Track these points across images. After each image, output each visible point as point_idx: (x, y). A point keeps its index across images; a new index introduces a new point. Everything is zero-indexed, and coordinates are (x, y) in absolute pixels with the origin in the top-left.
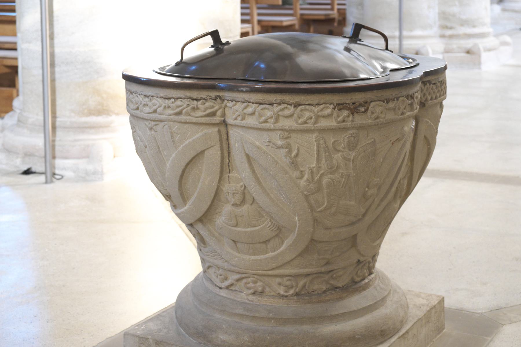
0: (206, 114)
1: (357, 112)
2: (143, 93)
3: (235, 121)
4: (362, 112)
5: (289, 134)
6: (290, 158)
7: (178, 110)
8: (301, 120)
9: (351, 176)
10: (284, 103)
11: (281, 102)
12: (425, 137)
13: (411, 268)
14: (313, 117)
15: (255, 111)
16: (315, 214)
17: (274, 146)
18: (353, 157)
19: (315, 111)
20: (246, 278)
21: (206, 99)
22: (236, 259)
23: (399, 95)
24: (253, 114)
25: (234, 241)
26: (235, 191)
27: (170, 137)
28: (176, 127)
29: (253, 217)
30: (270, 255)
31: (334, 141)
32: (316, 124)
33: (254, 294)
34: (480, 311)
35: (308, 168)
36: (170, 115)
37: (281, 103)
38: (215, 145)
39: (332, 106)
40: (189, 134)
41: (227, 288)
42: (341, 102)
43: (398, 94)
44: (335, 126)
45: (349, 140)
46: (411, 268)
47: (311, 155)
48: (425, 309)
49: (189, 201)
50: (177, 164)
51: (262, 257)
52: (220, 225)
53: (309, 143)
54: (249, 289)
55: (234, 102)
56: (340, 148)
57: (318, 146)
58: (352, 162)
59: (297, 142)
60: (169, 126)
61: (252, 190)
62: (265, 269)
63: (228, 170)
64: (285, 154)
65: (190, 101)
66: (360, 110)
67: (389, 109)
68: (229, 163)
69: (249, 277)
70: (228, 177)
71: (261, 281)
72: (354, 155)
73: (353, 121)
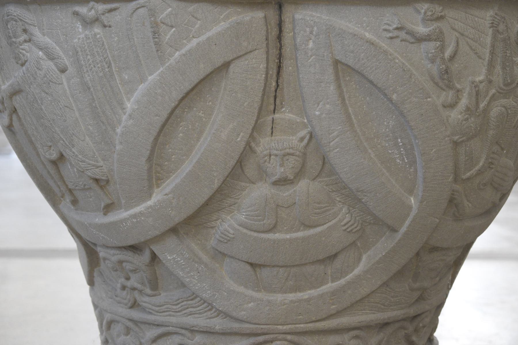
5: (443, 10)
17: (408, 37)
25: (251, 264)
26: (288, 151)
27: (150, 35)
29: (317, 205)
30: (329, 287)
38: (256, 50)
40: (197, 26)
49: (158, 187)
50: (159, 97)
51: (314, 293)
52: (232, 231)
53: (478, 31)
60: (150, 10)
61: (332, 144)
62: (314, 319)
63: (272, 107)
68: (276, 91)
70: (271, 122)
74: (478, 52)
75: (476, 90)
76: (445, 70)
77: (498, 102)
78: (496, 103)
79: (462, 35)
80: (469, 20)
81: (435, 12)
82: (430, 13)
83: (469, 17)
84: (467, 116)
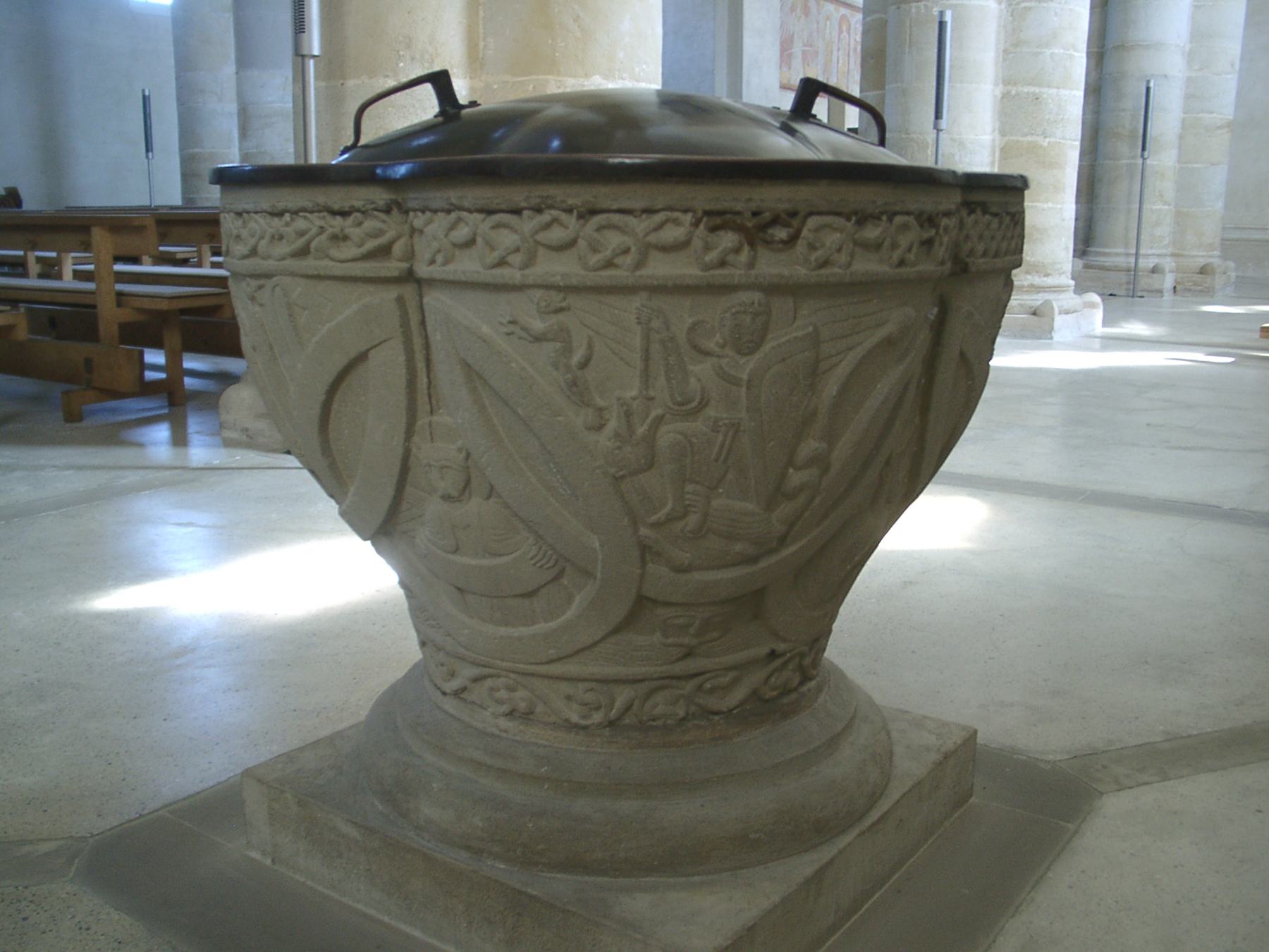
0: (365, 252)
2: (232, 207)
3: (432, 268)
7: (301, 242)
8: (594, 259)
9: (742, 428)
10: (551, 207)
12: (962, 354)
13: (913, 652)
14: (633, 249)
15: (475, 234)
16: (644, 531)
17: (524, 334)
20: (491, 676)
21: (363, 209)
22: (466, 631)
23: (898, 208)
24: (470, 243)
25: (459, 589)
28: (298, 289)
30: (541, 627)
31: (695, 324)
33: (510, 714)
34: (1051, 757)
35: (619, 399)
36: (283, 259)
37: (543, 206)
39: (688, 218)
41: (457, 694)
46: (913, 652)
48: (934, 757)
54: (500, 702)
55: (428, 214)
56: (711, 345)
57: (647, 338)
58: (744, 389)
61: (483, 460)
62: (533, 661)
63: (428, 408)
65: (324, 218)
67: (865, 246)
69: (499, 676)
71: (525, 687)
79: (597, 333)
82: (544, 304)
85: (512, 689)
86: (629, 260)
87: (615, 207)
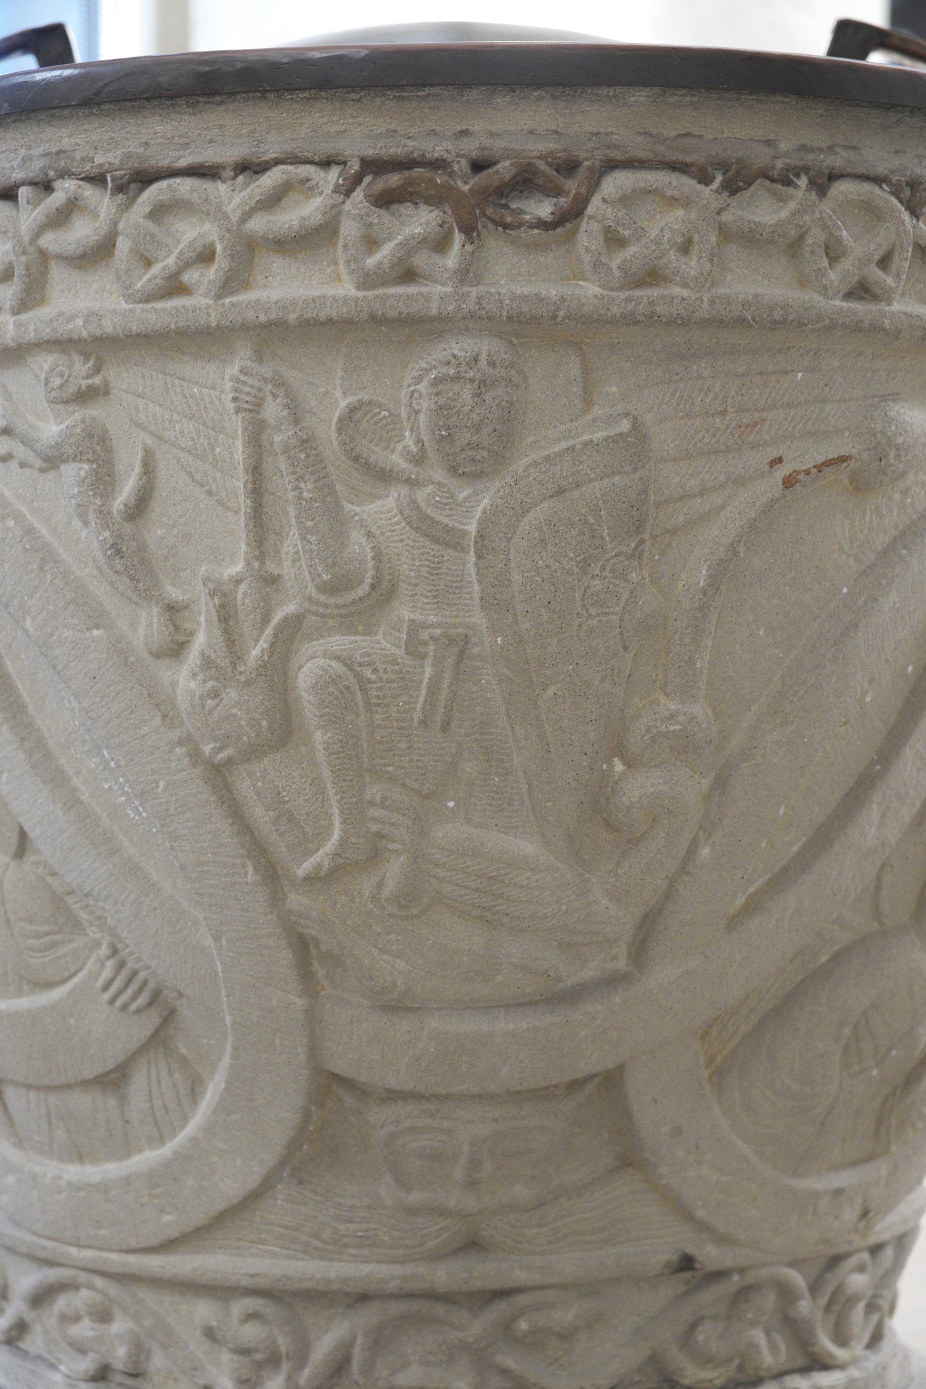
1: (496, 223)
4: (532, 227)
5: (97, 370)
6: (104, 515)
8: (145, 280)
11: (51, 168)
14: (219, 248)
18: (479, 523)
19: (229, 209)
23: (836, 161)
29: (29, 927)
31: (352, 410)
32: (233, 293)
37: (51, 174)
39: (333, 175)
42: (392, 151)
43: (821, 150)
44: (345, 300)
45: (442, 401)
47: (221, 503)
51: (112, 1169)
53: (205, 424)
54: (80, 1349)
56: (397, 460)
58: (472, 557)
59: (142, 417)
62: (133, 1243)
64: (73, 496)
66: (522, 212)
72: (484, 512)
73: (464, 275)
74: (214, 491)
75: (215, 605)
76: (112, 545)
77: (319, 645)
78: (314, 646)
80: (175, 393)
81: (70, 376)
82: (57, 382)
83: (173, 385)
84: (211, 683)
85: (103, 1316)
86: (211, 274)
87: (183, 163)
